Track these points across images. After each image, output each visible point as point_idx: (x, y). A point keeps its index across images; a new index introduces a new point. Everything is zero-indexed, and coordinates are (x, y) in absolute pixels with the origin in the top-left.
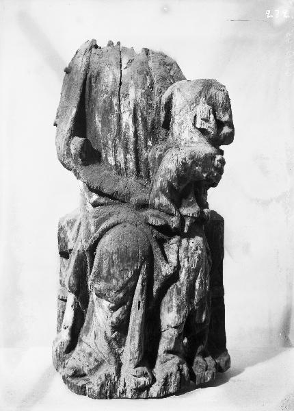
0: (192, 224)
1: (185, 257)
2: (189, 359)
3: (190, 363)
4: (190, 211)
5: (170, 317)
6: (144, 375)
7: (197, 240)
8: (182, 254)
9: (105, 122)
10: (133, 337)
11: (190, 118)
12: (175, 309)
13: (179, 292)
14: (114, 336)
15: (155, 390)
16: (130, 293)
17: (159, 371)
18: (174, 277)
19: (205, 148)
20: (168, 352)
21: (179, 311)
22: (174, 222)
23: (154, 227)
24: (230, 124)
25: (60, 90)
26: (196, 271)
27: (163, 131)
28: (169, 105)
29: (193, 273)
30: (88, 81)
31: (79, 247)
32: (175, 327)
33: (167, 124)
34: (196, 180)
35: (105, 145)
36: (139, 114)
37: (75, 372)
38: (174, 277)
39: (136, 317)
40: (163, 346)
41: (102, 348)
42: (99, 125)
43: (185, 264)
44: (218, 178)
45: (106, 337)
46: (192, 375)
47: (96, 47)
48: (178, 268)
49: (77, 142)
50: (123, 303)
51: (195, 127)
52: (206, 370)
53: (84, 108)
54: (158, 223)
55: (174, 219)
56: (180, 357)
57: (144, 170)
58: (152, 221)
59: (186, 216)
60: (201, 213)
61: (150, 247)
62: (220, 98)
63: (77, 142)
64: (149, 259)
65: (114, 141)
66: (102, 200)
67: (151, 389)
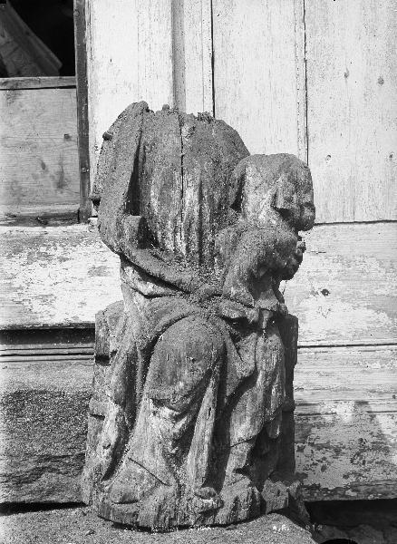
0: (270, 320)
1: (263, 357)
2: (258, 482)
3: (260, 489)
4: (267, 303)
5: (242, 429)
6: (210, 495)
7: (275, 339)
8: (256, 354)
9: (164, 199)
10: (200, 452)
11: (268, 196)
12: (248, 419)
13: (254, 398)
14: (174, 452)
15: (222, 516)
16: (197, 400)
17: (227, 495)
18: (248, 381)
19: (285, 234)
20: (238, 471)
21: (252, 422)
22: (252, 315)
23: (228, 320)
24: (311, 206)
25: (187, 75)
26: (274, 374)
27: (232, 212)
28: (242, 178)
29: (271, 376)
30: (141, 150)
31: (128, 347)
32: (247, 441)
33: (237, 205)
34: (275, 267)
35: (163, 226)
36: (205, 191)
37: (124, 498)
38: (248, 381)
39: (204, 428)
40: (232, 463)
41: (156, 463)
42: (155, 203)
43: (262, 365)
44: (296, 269)
45: (164, 454)
46: (263, 503)
47: (148, 111)
48: (254, 374)
49: (133, 221)
50: (189, 410)
51: (275, 208)
52: (278, 496)
53: (137, 181)
54: (235, 315)
55: (252, 311)
56: (251, 479)
57: (204, 257)
58: (225, 313)
59: (264, 309)
60: (279, 307)
61: (225, 344)
62: (302, 177)
63: (133, 221)
64: (223, 357)
65: (175, 221)
66: (161, 290)
67: (219, 514)
